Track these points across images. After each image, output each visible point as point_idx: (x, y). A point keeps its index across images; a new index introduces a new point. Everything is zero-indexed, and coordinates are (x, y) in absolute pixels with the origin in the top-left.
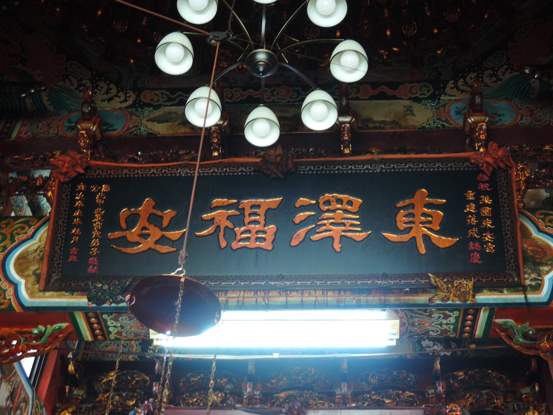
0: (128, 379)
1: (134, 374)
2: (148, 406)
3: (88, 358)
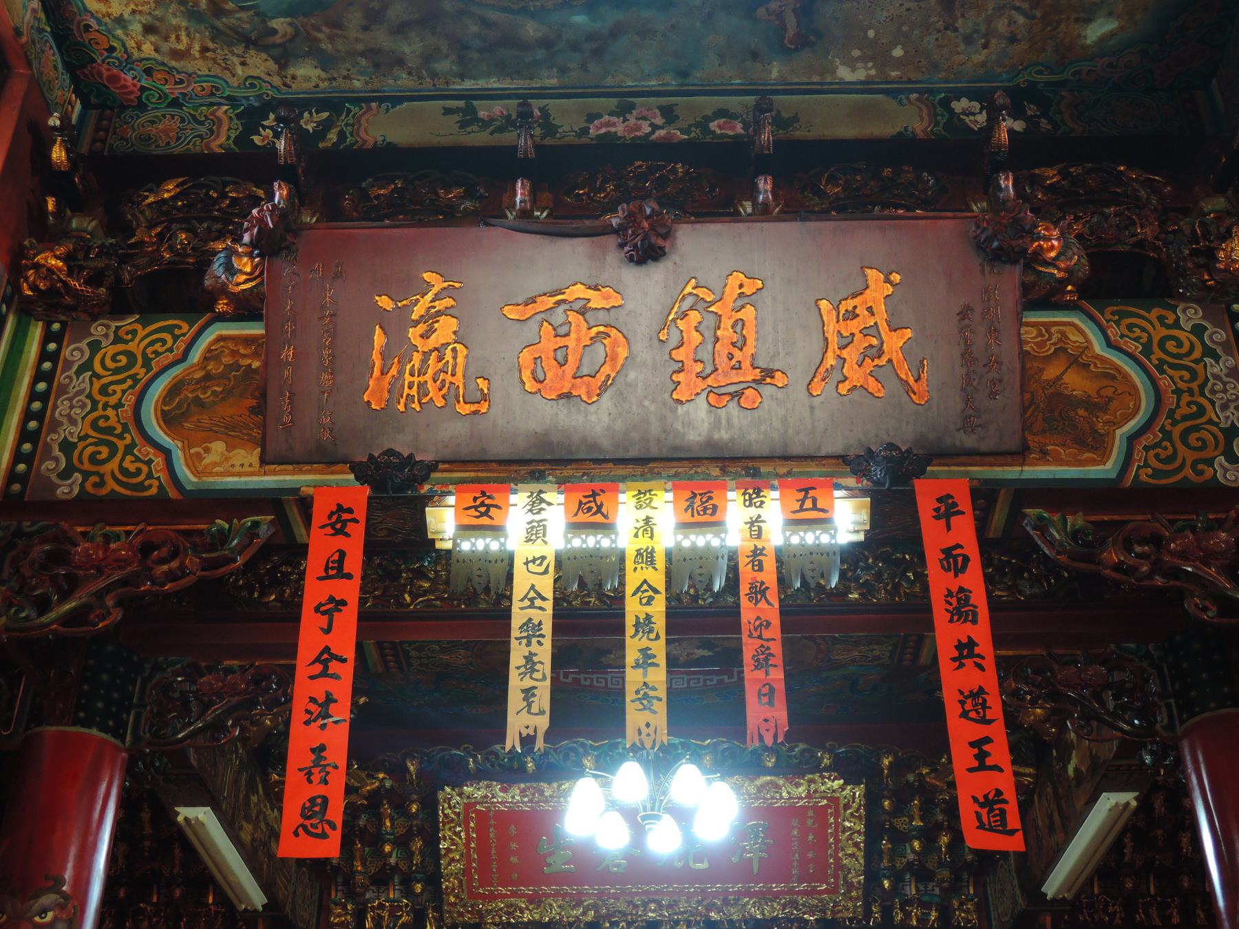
0: (211, 196)
1: (225, 184)
2: (261, 221)
3: (106, 149)
